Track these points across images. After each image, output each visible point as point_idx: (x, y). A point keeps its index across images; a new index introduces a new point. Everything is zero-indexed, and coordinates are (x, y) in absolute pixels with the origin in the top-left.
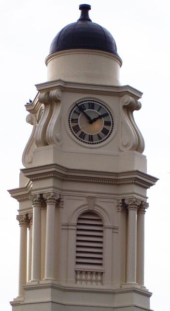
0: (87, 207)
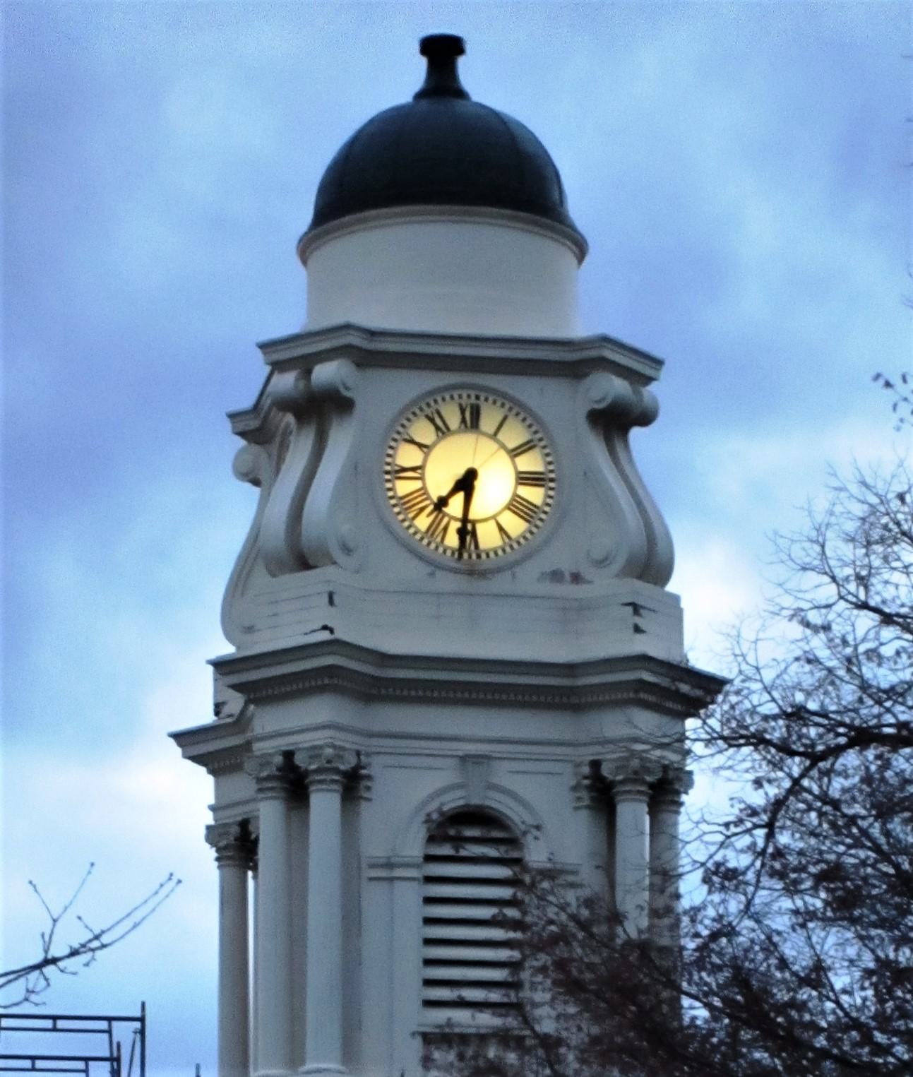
0: (459, 793)
